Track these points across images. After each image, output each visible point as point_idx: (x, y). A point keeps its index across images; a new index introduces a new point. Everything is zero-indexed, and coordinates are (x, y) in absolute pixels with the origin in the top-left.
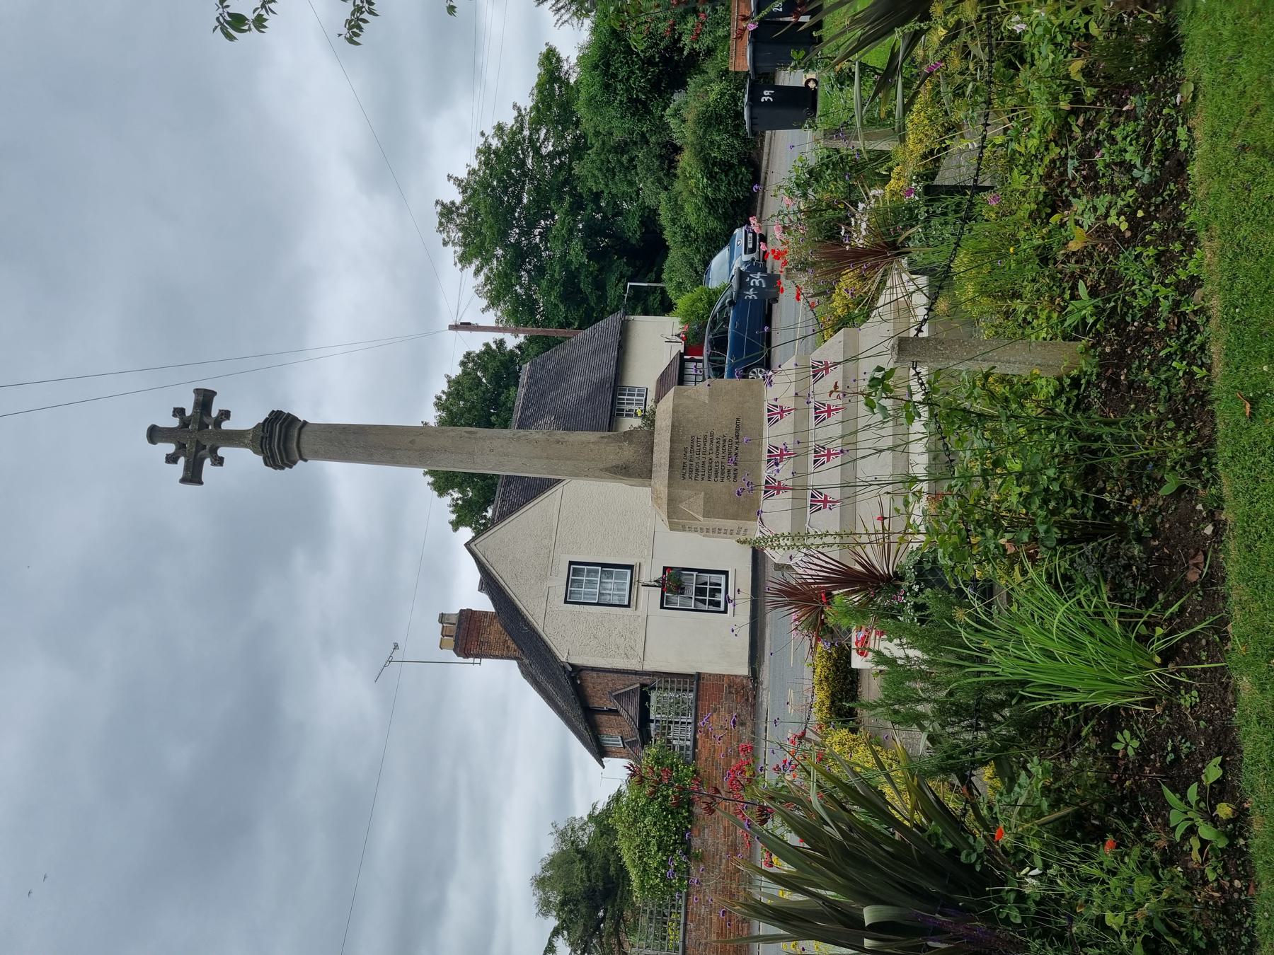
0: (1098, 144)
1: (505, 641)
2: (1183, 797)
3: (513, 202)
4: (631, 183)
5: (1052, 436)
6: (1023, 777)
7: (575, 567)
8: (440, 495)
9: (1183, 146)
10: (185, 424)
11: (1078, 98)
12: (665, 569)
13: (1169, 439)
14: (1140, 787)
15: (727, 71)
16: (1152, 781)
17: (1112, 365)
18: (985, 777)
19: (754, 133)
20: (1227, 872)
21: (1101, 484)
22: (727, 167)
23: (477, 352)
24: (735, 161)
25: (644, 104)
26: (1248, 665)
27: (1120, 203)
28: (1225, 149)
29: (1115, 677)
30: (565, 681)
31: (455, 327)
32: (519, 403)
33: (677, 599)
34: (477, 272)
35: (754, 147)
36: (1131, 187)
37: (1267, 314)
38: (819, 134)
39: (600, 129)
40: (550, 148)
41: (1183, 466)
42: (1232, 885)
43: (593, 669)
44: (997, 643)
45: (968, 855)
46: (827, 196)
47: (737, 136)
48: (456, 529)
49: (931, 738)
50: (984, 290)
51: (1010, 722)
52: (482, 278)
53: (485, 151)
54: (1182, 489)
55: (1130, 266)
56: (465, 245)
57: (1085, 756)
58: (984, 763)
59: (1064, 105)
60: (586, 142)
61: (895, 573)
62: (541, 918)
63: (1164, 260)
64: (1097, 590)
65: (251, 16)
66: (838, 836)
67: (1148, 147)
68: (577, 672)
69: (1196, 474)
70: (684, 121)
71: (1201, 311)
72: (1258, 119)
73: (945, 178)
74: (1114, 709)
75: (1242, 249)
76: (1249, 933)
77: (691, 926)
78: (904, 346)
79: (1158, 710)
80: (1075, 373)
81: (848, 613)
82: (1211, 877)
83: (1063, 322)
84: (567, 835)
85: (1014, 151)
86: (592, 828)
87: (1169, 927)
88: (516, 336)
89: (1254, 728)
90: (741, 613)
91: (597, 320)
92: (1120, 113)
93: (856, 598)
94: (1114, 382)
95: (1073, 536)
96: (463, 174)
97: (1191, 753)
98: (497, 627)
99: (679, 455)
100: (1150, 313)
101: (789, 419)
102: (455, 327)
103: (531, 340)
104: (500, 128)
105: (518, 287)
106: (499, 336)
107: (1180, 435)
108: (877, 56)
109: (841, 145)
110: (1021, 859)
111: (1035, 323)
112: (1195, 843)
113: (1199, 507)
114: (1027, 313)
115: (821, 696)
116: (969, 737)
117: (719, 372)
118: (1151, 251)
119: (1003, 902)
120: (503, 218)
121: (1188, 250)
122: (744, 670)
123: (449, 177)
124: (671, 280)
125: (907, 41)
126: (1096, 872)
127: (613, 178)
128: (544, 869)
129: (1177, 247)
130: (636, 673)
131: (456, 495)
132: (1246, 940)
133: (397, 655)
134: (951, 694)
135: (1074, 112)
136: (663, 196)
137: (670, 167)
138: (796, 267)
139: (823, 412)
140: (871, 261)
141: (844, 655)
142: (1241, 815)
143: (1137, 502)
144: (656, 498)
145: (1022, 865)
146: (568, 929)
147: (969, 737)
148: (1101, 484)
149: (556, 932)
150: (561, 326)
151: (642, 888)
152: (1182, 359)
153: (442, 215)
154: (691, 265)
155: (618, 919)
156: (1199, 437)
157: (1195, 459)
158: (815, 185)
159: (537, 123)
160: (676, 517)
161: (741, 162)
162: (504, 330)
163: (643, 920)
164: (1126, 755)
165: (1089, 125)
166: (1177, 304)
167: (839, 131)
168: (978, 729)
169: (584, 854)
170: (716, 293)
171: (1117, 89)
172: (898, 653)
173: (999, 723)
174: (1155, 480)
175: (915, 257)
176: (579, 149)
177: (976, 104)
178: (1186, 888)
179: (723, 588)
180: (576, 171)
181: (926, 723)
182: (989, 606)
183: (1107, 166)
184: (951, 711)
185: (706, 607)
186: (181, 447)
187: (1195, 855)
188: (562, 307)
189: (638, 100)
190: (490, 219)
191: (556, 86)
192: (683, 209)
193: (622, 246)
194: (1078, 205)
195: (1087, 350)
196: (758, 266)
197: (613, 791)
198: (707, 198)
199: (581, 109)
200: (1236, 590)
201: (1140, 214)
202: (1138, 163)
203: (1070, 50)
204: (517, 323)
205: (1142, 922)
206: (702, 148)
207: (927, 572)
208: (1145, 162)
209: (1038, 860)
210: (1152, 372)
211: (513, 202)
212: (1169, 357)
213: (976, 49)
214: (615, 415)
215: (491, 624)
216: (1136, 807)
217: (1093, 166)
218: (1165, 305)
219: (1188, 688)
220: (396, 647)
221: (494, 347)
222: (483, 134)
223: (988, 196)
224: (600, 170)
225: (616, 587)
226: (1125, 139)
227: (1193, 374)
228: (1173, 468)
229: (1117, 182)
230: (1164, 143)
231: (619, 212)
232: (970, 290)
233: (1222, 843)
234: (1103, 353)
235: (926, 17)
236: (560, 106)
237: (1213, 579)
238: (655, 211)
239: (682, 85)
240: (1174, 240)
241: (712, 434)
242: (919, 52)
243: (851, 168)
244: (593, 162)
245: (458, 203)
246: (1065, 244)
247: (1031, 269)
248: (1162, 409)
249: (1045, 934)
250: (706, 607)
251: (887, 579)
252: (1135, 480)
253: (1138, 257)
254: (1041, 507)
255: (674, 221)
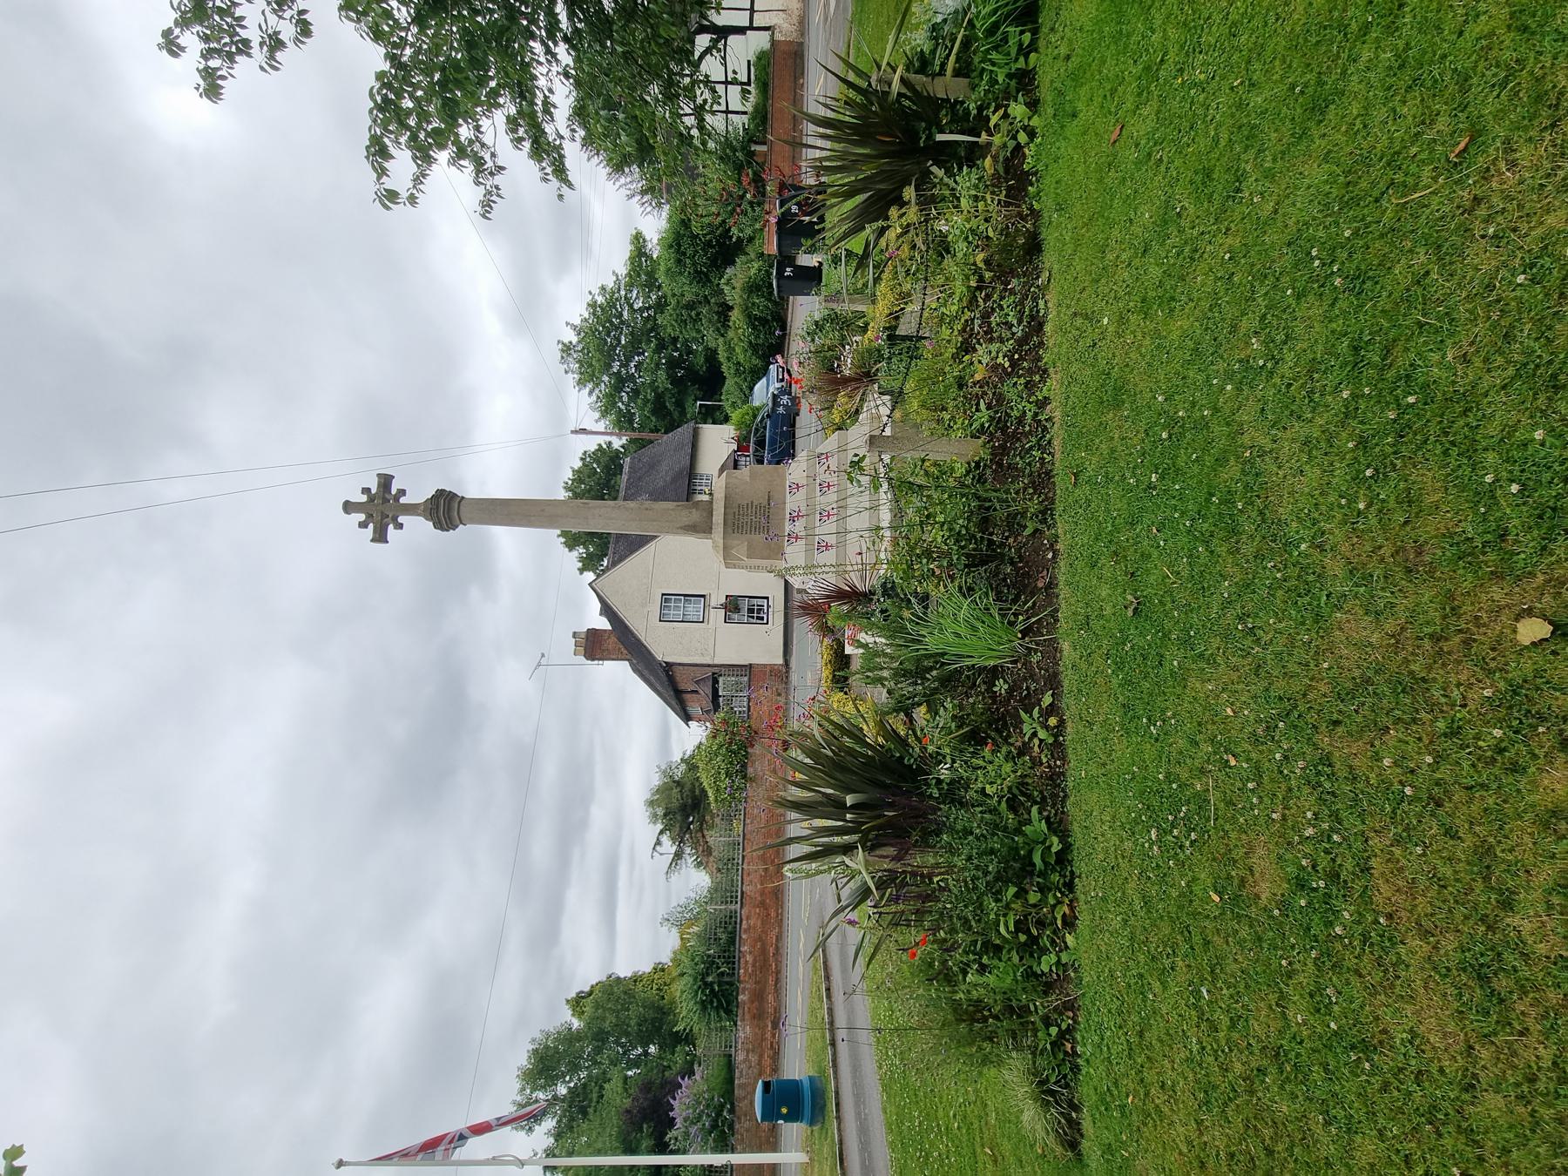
0: (993, 309)
1: (620, 649)
2: (1031, 716)
3: (615, 343)
4: (698, 331)
5: (964, 499)
6: (942, 711)
7: (666, 597)
8: (570, 550)
9: (1042, 312)
10: (371, 499)
11: (981, 279)
12: (727, 596)
13: (1030, 500)
14: (1007, 711)
15: (762, 254)
16: (1015, 708)
17: (999, 453)
18: (921, 713)
19: (781, 298)
20: (1053, 756)
21: (991, 530)
22: (763, 321)
23: (593, 450)
24: (769, 318)
25: (706, 275)
26: (1068, 635)
27: (1005, 349)
28: (1065, 314)
29: (996, 647)
30: (663, 675)
31: (575, 432)
32: (623, 485)
33: (736, 616)
34: (591, 393)
35: (783, 309)
36: (1012, 338)
37: (1085, 421)
38: (822, 297)
39: (676, 291)
40: (641, 305)
41: (1037, 517)
42: (1055, 764)
43: (680, 664)
44: (928, 630)
45: (909, 760)
46: (828, 342)
47: (770, 300)
48: (581, 573)
49: (889, 692)
50: (923, 405)
51: (935, 679)
52: (594, 398)
53: (593, 305)
54: (1036, 530)
55: (1009, 392)
56: (581, 373)
57: (977, 696)
58: (920, 705)
59: (973, 284)
60: (666, 301)
61: (870, 591)
62: (651, 825)
63: (1029, 386)
64: (987, 594)
65: (404, 194)
66: (830, 754)
67: (1022, 313)
68: (669, 666)
69: (1044, 521)
70: (734, 288)
71: (1049, 420)
72: (1084, 295)
73: (901, 331)
74: (995, 667)
75: (1073, 380)
76: (1063, 790)
77: (748, 821)
78: (873, 441)
79: (1019, 666)
80: (977, 459)
81: (840, 617)
82: (1044, 760)
83: (971, 425)
84: (667, 773)
85: (943, 313)
86: (683, 767)
87: (1020, 791)
88: (620, 439)
89: (1069, 672)
90: (777, 619)
91: (678, 427)
92: (1005, 290)
93: (845, 607)
94: (1000, 464)
95: (974, 562)
96: (577, 322)
97: (1036, 690)
98: (613, 639)
99: (730, 517)
100: (1021, 420)
101: (803, 491)
102: (575, 432)
103: (631, 441)
104: (603, 288)
105: (620, 404)
106: (608, 438)
107: (1035, 497)
108: (856, 244)
109: (834, 306)
110: (938, 758)
111: (955, 427)
112: (1036, 741)
113: (1046, 542)
114: (950, 420)
115: (826, 673)
116: (911, 689)
117: (760, 462)
118: (1022, 381)
119: (929, 785)
120: (608, 356)
121: (1043, 380)
122: (781, 661)
123: (567, 324)
124: (727, 399)
125: (875, 235)
126: (981, 763)
127: (686, 327)
128: (653, 795)
129: (1037, 378)
130: (709, 666)
131: (581, 551)
132: (1061, 794)
133: (544, 661)
134: (901, 664)
135: (979, 288)
136: (721, 340)
137: (725, 321)
138: (808, 390)
139: (825, 487)
140: (854, 385)
141: (841, 646)
142: (1062, 722)
143: (1011, 540)
144: (715, 547)
145: (941, 762)
146: (669, 830)
147: (911, 689)
148: (991, 530)
149: (661, 832)
150: (652, 431)
151: (716, 801)
152: (1038, 449)
153: (563, 351)
154: (741, 390)
155: (702, 821)
156: (1047, 498)
157: (1043, 512)
158: (820, 334)
159: (630, 286)
160: (729, 559)
161: (774, 319)
162: (611, 434)
163: (717, 820)
164: (1001, 694)
165: (988, 297)
166: (1036, 414)
167: (835, 297)
168: (917, 684)
169: (678, 783)
170: (758, 409)
171: (1004, 273)
172: (870, 640)
173: (929, 680)
174: (1021, 526)
175: (882, 383)
176: (660, 306)
177: (918, 280)
178: (1030, 768)
179: (765, 608)
180: (659, 322)
181: (886, 683)
182: (926, 607)
183: (998, 325)
184: (899, 674)
185: (755, 621)
186: (370, 516)
187: (1036, 749)
188: (653, 419)
189: (701, 272)
190: (598, 355)
191: (643, 259)
192: (734, 350)
193: (692, 374)
194: (980, 350)
195: (985, 444)
196: (786, 391)
197: (696, 743)
198: (750, 342)
199: (661, 278)
200: (1063, 591)
201: (1016, 356)
202: (1015, 322)
203: (977, 247)
204: (620, 429)
205: (1006, 789)
206: (747, 308)
207: (888, 589)
208: (1020, 322)
209: (948, 759)
210: (1021, 458)
211: (615, 343)
212: (1031, 448)
213: (919, 243)
214: (690, 492)
215: (609, 637)
216: (1005, 725)
217: (989, 324)
218: (1029, 415)
219: (1036, 651)
220: (543, 655)
221: (605, 446)
222: (590, 293)
223: (926, 343)
224: (676, 321)
225: (694, 610)
226: (1008, 307)
227: (1044, 459)
228: (1031, 518)
229: (1003, 335)
230: (1031, 311)
231: (690, 352)
232: (915, 404)
233: (1051, 741)
234: (994, 446)
235: (887, 218)
236: (647, 274)
237: (1051, 585)
238: (716, 350)
239: (733, 263)
240: (1036, 373)
241: (752, 503)
242: (883, 242)
243: (843, 323)
244: (671, 315)
245: (574, 342)
246: (972, 376)
247: (954, 391)
248: (1026, 481)
249: (952, 801)
250: (755, 621)
251: (864, 595)
252: (1010, 526)
253: (1015, 383)
254: (954, 544)
255: (728, 359)
